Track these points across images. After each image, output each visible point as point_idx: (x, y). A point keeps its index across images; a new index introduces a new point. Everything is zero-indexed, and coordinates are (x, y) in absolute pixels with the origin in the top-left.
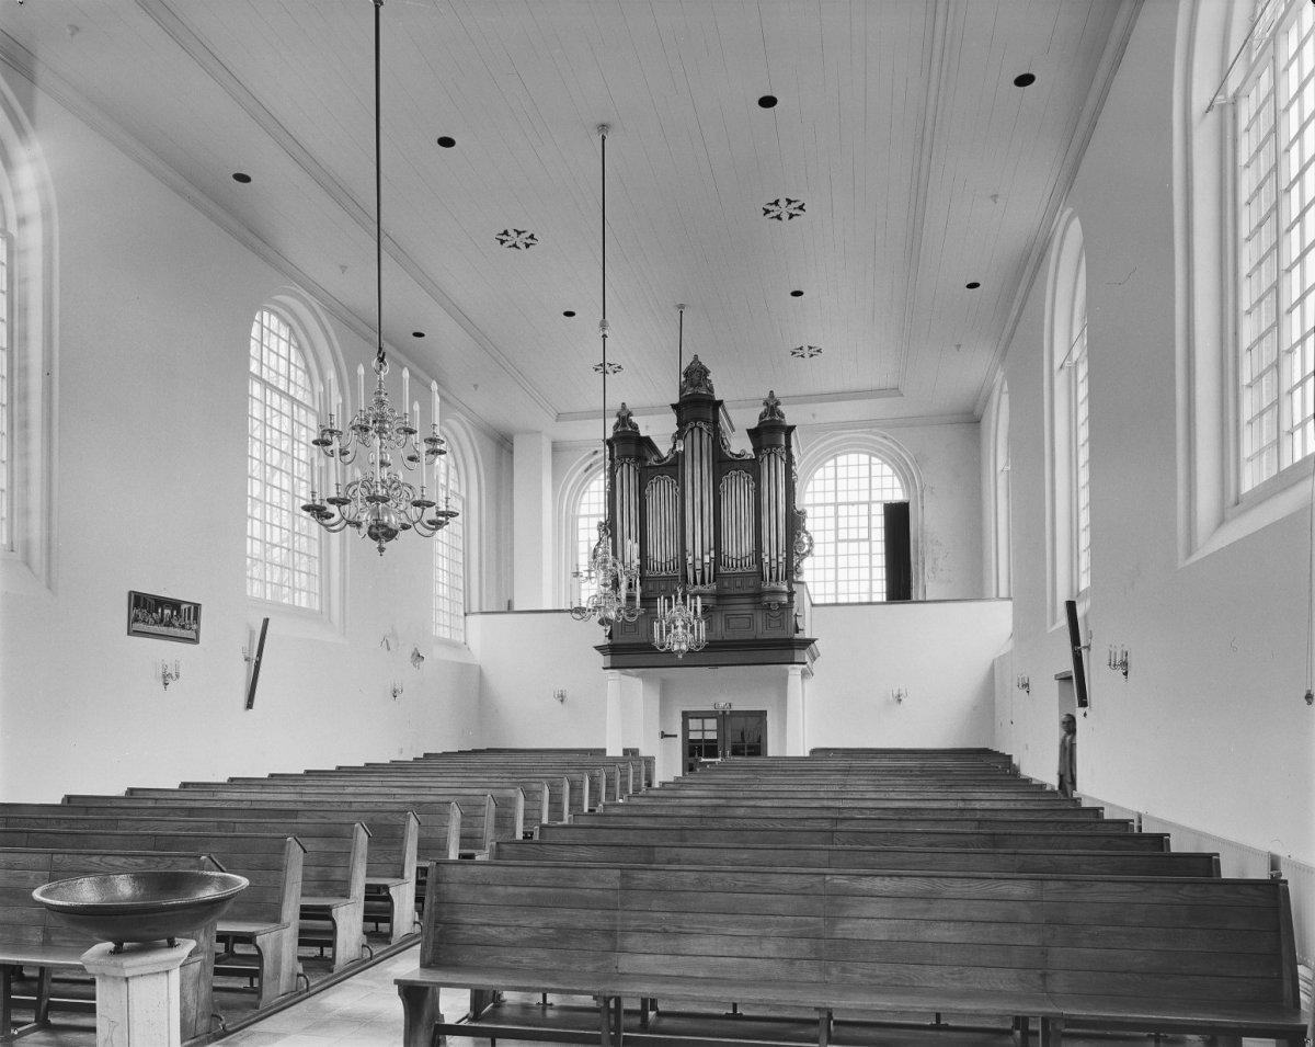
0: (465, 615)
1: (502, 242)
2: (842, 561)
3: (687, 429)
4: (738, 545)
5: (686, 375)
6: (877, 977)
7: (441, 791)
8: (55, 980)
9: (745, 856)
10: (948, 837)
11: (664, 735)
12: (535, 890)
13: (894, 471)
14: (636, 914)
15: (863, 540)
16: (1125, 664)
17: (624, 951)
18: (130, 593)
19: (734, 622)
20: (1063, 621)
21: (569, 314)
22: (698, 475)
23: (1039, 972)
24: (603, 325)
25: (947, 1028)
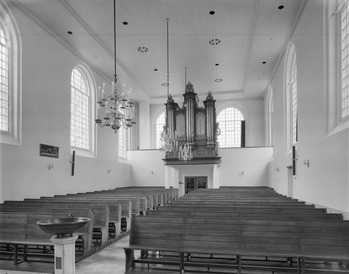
0: (127, 151)
1: (139, 50)
2: (227, 136)
3: (187, 101)
4: (201, 132)
5: (187, 86)
6: (254, 247)
7: (125, 198)
8: (242, 260)
9: (214, 215)
10: (267, 210)
11: (180, 183)
12: (160, 224)
13: (241, 112)
14: (188, 230)
15: (227, 131)
16: (308, 164)
17: (184, 240)
18: (41, 144)
19: (199, 153)
20: (291, 151)
21: (156, 70)
22: (189, 113)
23: (298, 245)
24: (168, 72)
25: (269, 261)
